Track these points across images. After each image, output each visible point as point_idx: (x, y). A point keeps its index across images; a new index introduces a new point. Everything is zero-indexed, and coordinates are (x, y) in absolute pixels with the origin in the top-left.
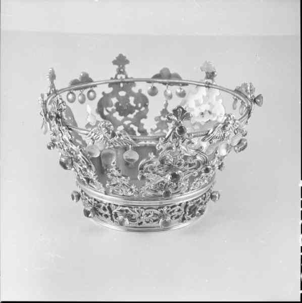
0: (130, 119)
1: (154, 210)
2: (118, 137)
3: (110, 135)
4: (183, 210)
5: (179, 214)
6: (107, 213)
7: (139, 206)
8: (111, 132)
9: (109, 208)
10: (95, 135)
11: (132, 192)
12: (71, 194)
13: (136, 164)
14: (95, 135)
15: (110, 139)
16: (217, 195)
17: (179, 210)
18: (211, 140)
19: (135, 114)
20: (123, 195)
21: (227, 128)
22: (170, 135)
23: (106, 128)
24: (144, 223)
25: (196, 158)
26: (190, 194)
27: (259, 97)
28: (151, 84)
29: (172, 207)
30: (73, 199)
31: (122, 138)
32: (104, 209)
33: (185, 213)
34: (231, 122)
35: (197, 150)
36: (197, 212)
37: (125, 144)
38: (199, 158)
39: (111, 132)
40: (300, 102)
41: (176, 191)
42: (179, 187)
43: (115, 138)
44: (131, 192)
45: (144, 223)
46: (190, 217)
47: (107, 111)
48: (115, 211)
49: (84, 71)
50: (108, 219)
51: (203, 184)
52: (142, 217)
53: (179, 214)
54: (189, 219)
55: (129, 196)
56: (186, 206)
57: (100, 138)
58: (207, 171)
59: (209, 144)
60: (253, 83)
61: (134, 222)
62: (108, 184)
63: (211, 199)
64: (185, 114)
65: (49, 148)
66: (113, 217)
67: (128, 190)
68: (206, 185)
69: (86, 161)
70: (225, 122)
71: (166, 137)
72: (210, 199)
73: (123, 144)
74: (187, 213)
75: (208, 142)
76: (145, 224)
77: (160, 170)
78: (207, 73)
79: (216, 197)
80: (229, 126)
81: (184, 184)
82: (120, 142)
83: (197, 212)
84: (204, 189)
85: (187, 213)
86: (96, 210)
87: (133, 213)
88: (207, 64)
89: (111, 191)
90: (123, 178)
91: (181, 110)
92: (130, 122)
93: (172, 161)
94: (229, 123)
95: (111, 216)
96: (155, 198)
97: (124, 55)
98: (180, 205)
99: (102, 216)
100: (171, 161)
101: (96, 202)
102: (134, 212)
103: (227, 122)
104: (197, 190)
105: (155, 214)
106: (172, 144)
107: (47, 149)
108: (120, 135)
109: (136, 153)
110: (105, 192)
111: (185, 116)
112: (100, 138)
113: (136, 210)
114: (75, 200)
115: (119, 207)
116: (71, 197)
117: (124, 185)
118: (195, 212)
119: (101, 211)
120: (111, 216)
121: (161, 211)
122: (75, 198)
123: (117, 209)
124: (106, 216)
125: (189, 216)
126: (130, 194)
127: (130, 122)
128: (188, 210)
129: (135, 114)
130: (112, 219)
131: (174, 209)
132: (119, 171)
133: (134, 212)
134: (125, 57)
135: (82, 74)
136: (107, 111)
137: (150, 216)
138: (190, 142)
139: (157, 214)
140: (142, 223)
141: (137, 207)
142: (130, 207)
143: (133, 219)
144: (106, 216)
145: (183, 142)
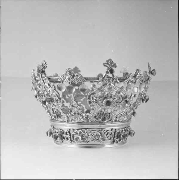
0: (81, 101)
2: (76, 77)
3: (72, 77)
6: (68, 136)
7: (88, 128)
10: (63, 78)
11: (83, 119)
12: (46, 132)
14: (63, 78)
19: (83, 99)
23: (70, 72)
24: (90, 141)
27: (154, 70)
28: (92, 83)
30: (47, 135)
31: (78, 78)
32: (66, 134)
37: (80, 81)
41: (110, 120)
42: (111, 116)
44: (82, 119)
47: (68, 96)
48: (73, 133)
49: (56, 73)
55: (81, 122)
57: (66, 79)
58: (126, 101)
61: (85, 140)
63: (130, 135)
66: (72, 139)
67: (81, 117)
71: (103, 77)
72: (129, 135)
74: (116, 137)
77: (100, 100)
78: (124, 73)
86: (60, 136)
91: (111, 61)
92: (80, 103)
94: (137, 74)
96: (97, 123)
97: (78, 67)
102: (85, 133)
104: (121, 123)
106: (107, 81)
107: (35, 98)
113: (85, 131)
115: (75, 130)
116: (46, 134)
120: (70, 137)
122: (49, 134)
125: (118, 140)
127: (80, 103)
129: (83, 99)
133: (85, 133)
134: (78, 68)
135: (54, 74)
136: (68, 96)
140: (89, 141)
141: (86, 129)
145: (113, 81)
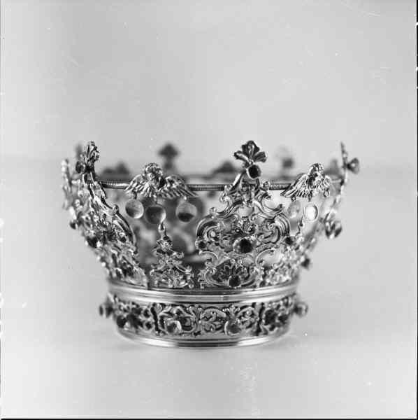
1: (217, 310)
3: (158, 184)
4: (257, 314)
5: (253, 320)
6: (151, 319)
7: (197, 303)
8: (160, 178)
9: (153, 310)
10: (137, 185)
11: (186, 282)
13: (188, 250)
14: (137, 185)
15: (158, 188)
16: (304, 307)
17: (253, 315)
18: (294, 196)
20: (173, 288)
21: (315, 183)
22: (239, 181)
25: (274, 222)
26: (265, 290)
27: (355, 161)
29: (242, 308)
31: (174, 186)
32: (146, 315)
33: (261, 320)
34: (319, 174)
35: (276, 210)
36: (277, 321)
38: (277, 223)
39: (160, 178)
40: (415, 15)
42: (251, 274)
43: (166, 187)
45: (203, 331)
46: (268, 329)
48: (161, 314)
50: (151, 330)
51: (284, 279)
52: (200, 322)
53: (253, 320)
54: (266, 333)
55: (181, 289)
56: (262, 309)
57: (145, 189)
59: (291, 201)
60: (344, 143)
62: (153, 271)
64: (258, 153)
65: (73, 226)
66: (160, 327)
67: (181, 277)
68: (287, 283)
69: (123, 227)
70: (311, 174)
73: (175, 194)
74: (264, 321)
75: (290, 199)
76: (205, 336)
77: (226, 239)
79: (301, 309)
80: (317, 179)
81: (258, 270)
82: (172, 193)
83: (277, 321)
84: (285, 288)
85: (264, 321)
86: (132, 320)
87: (187, 315)
88: (284, 149)
89: (156, 282)
90: (175, 253)
93: (242, 223)
94: (316, 175)
95: (156, 323)
96: (219, 290)
98: (253, 305)
99: (142, 326)
100: (240, 225)
101: (134, 306)
103: (314, 173)
105: (217, 319)
106: (242, 195)
108: (171, 182)
109: (193, 206)
110: (148, 284)
111: (257, 156)
112: (145, 189)
113: (191, 309)
114: (104, 315)
115: (167, 307)
117: (174, 268)
118: (274, 321)
119: (142, 318)
120: (156, 323)
121: (228, 313)
123: (165, 311)
124: (149, 326)
125: (267, 327)
126: (183, 284)
128: (264, 316)
130: (157, 329)
131: (244, 310)
132: (169, 241)
137: (211, 320)
138: (265, 195)
139: (222, 318)
140: (199, 333)
141: (192, 304)
142: (181, 304)
143: (188, 326)
144: (149, 326)
145: (256, 194)
